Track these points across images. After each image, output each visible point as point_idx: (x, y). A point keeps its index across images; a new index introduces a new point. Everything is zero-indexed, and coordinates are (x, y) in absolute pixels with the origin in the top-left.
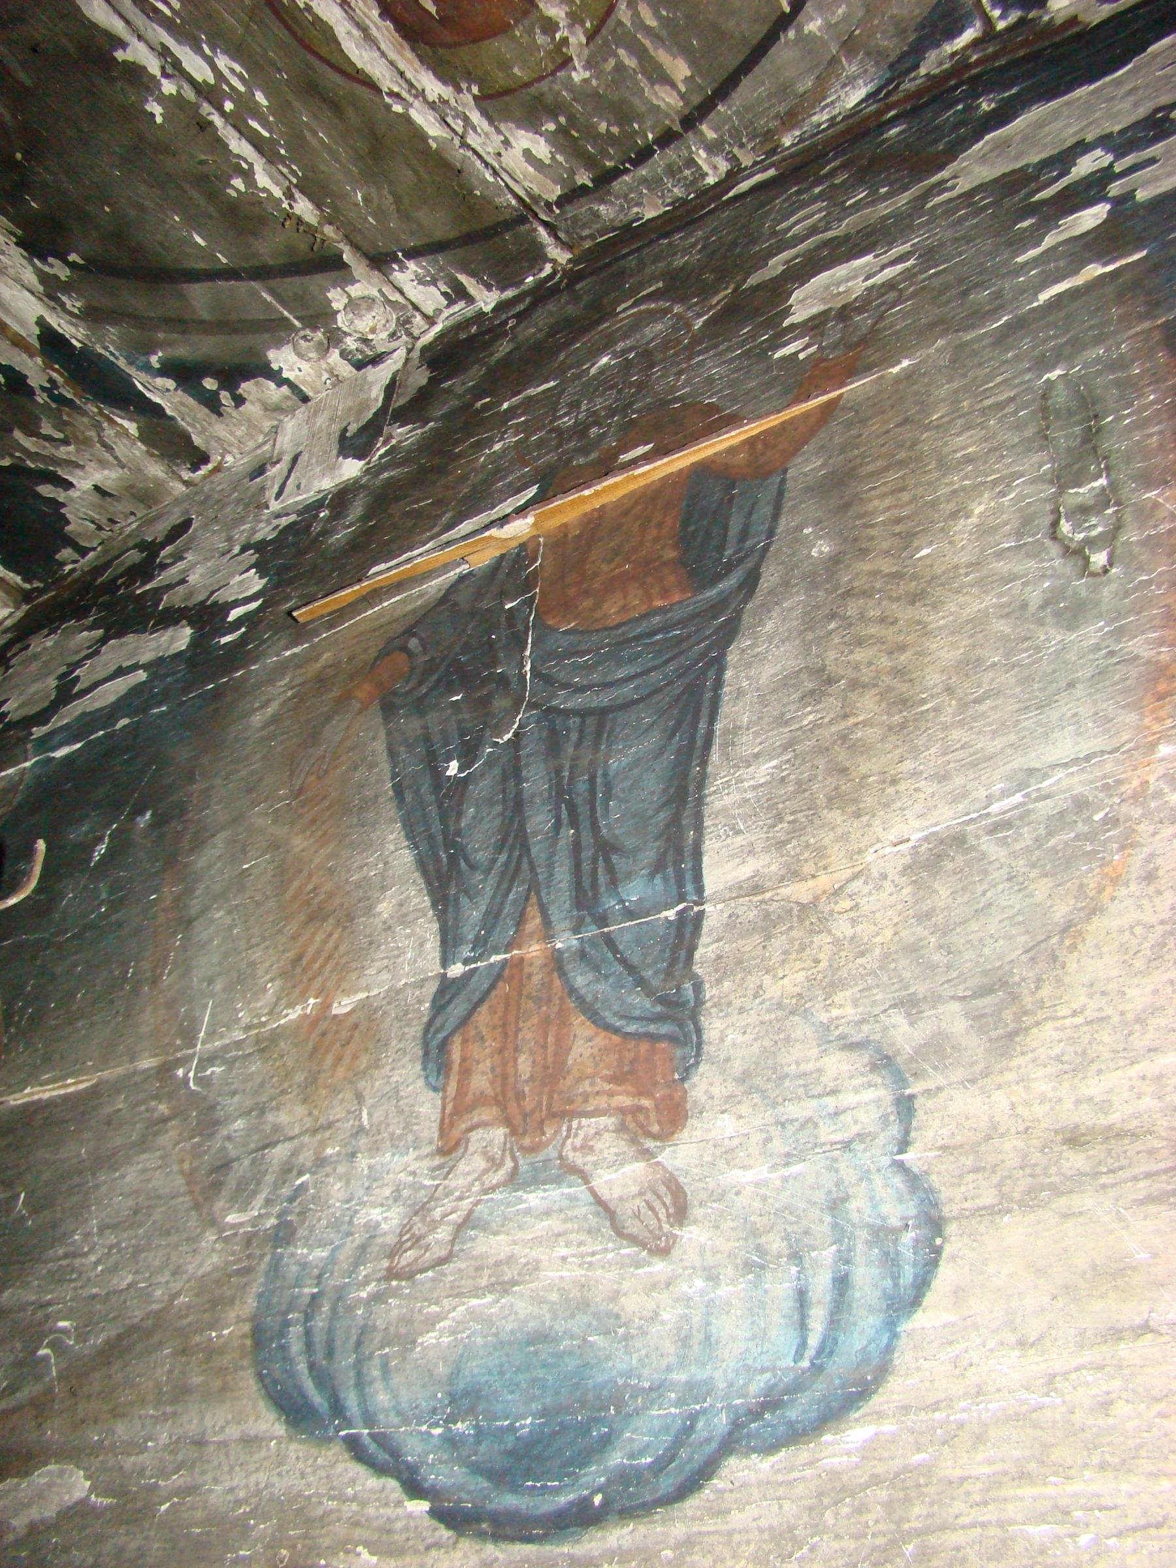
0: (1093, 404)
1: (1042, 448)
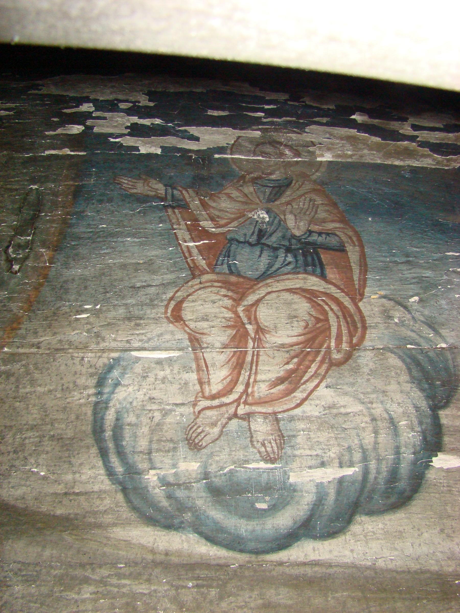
0: (41, 205)
1: (17, 215)
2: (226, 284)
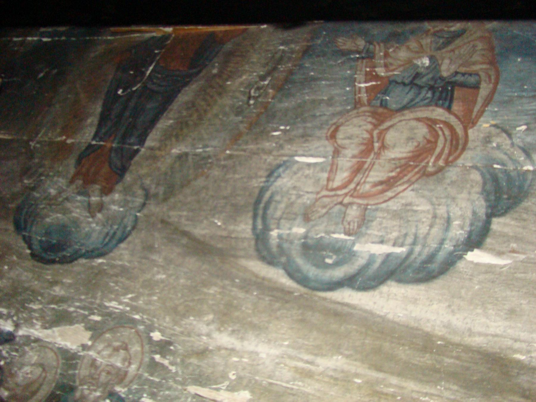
2: (374, 114)
